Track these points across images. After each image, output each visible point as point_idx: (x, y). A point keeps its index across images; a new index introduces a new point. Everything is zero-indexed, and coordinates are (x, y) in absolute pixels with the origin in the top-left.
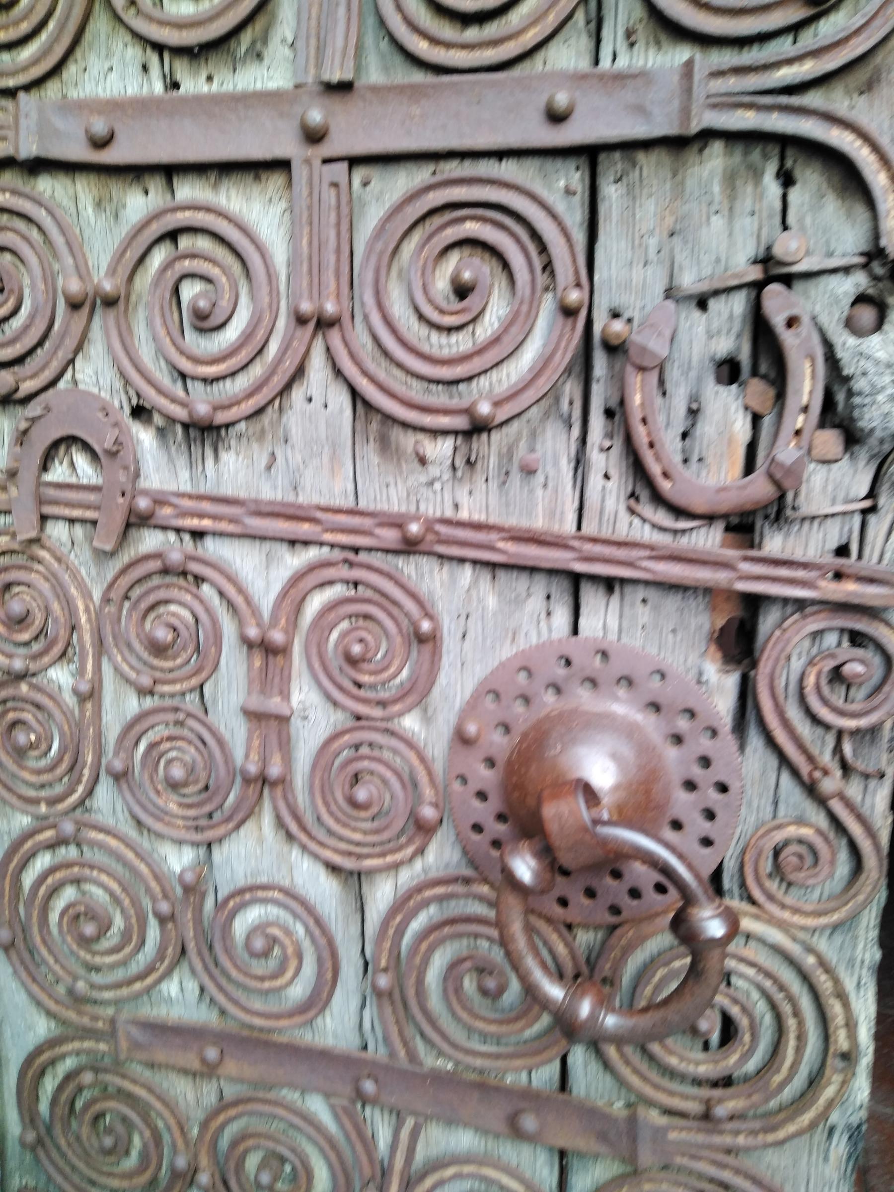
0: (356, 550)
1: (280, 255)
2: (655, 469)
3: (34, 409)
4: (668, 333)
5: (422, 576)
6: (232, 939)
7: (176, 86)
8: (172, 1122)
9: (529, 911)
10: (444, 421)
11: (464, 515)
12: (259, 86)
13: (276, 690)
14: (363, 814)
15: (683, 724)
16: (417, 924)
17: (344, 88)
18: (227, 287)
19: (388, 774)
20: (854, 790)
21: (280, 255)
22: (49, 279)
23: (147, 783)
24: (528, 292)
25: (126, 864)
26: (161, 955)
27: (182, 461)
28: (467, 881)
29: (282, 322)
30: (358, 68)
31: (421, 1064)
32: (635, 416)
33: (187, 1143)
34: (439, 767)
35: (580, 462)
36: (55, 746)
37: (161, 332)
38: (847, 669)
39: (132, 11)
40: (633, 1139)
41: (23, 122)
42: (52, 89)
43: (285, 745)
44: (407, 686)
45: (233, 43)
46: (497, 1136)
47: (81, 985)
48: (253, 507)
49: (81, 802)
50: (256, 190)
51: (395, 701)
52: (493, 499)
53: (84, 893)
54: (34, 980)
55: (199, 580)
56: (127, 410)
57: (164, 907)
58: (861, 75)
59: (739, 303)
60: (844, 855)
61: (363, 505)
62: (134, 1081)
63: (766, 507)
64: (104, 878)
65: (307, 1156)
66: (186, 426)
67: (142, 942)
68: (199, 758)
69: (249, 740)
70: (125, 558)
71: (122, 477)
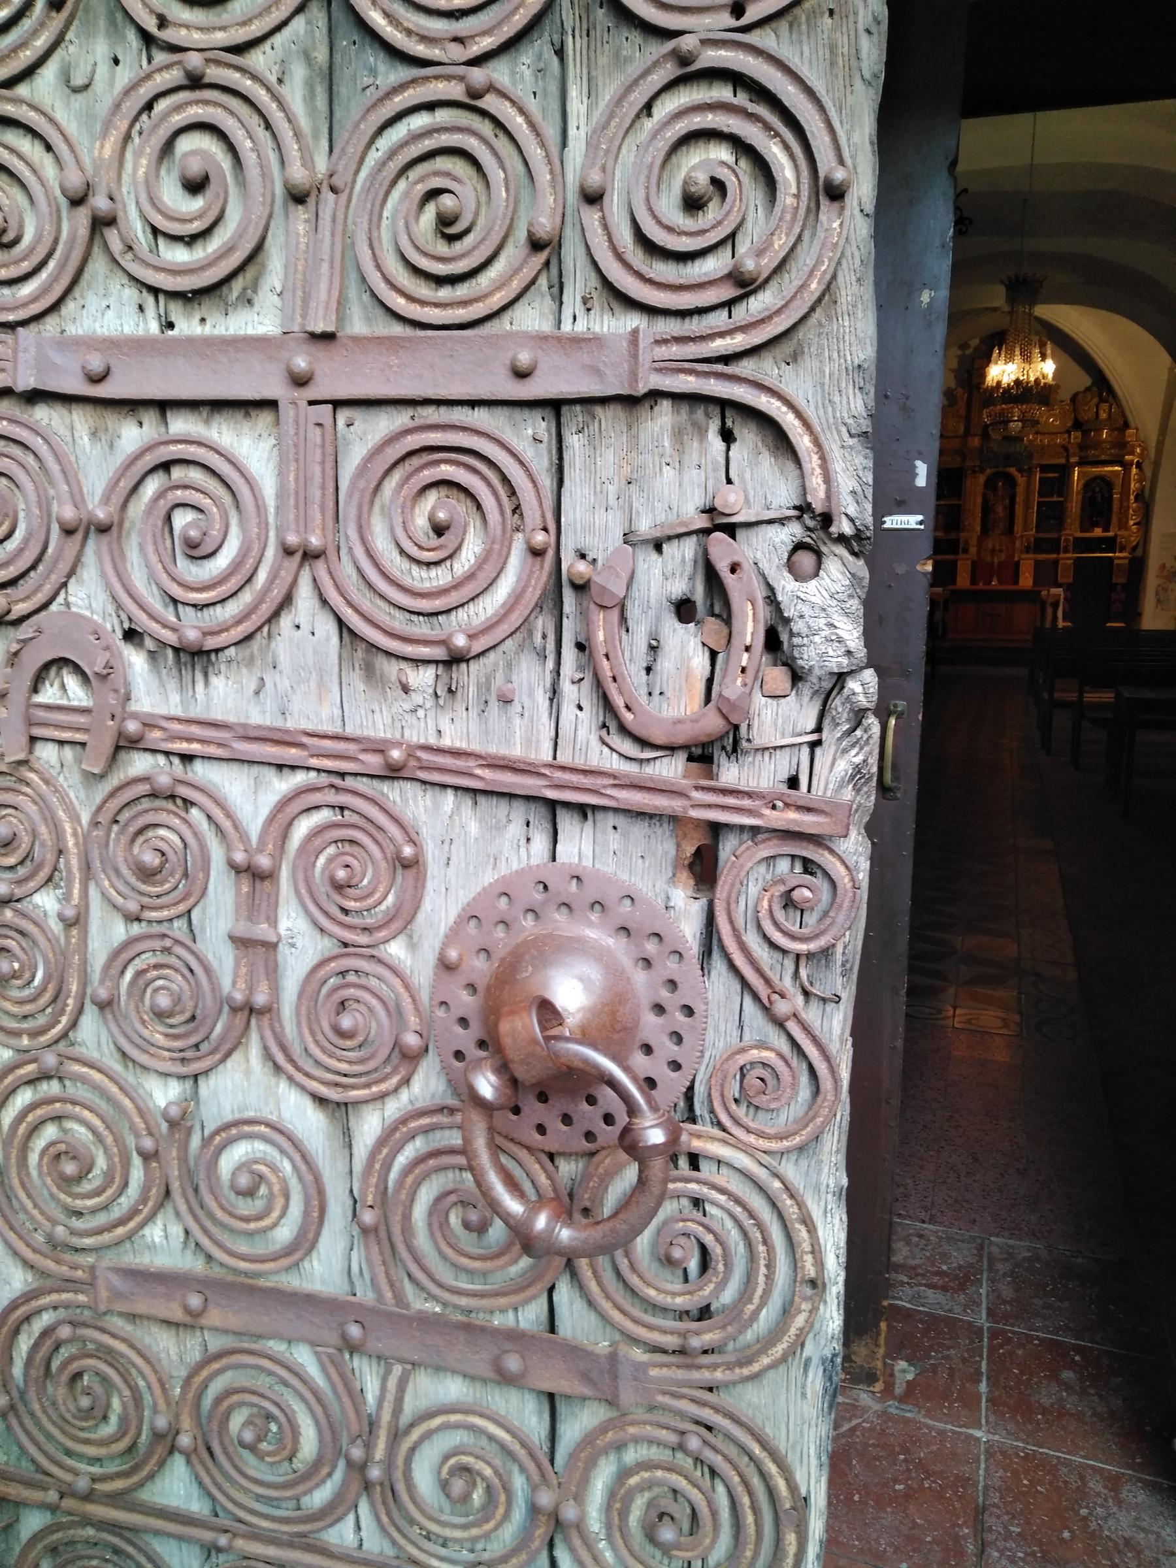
0: (342, 775)
1: (269, 488)
2: (619, 701)
3: (26, 631)
4: (625, 576)
5: (407, 801)
6: (218, 1178)
7: (171, 326)
8: (153, 1379)
9: (491, 1130)
10: (425, 651)
11: (446, 742)
12: (242, 332)
13: (263, 916)
14: (348, 1043)
15: (651, 947)
16: (402, 1160)
17: (328, 337)
18: (217, 517)
19: (374, 1002)
20: (812, 1014)
21: (269, 488)
22: (44, 504)
23: (133, 1014)
24: (499, 532)
25: (110, 1099)
26: (144, 1199)
27: (172, 685)
28: (452, 1111)
29: (271, 552)
30: (341, 318)
31: (407, 1306)
32: (601, 650)
33: (168, 1404)
34: (424, 997)
35: (555, 693)
36: (40, 975)
37: (154, 559)
38: (796, 895)
39: (129, 256)
40: (615, 1376)
41: (22, 356)
42: (51, 325)
43: (273, 973)
44: (392, 913)
45: (225, 289)
46: (484, 1381)
47: (60, 1230)
48: (241, 732)
49: (65, 1035)
50: (246, 426)
51: (379, 928)
52: (474, 727)
53: (65, 1131)
54: (12, 1228)
55: (188, 803)
56: (119, 634)
57: (148, 1144)
58: (787, 348)
59: (688, 549)
60: (804, 1079)
61: (350, 731)
62: (114, 1336)
63: (721, 738)
64: (86, 1114)
65: (294, 1411)
66: (176, 650)
67: (126, 1185)
68: (186, 987)
69: (237, 966)
70: (114, 781)
71: (112, 700)
